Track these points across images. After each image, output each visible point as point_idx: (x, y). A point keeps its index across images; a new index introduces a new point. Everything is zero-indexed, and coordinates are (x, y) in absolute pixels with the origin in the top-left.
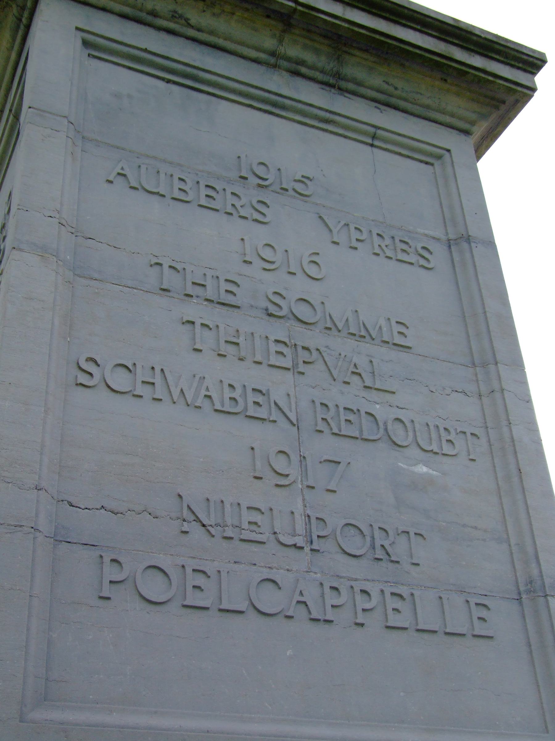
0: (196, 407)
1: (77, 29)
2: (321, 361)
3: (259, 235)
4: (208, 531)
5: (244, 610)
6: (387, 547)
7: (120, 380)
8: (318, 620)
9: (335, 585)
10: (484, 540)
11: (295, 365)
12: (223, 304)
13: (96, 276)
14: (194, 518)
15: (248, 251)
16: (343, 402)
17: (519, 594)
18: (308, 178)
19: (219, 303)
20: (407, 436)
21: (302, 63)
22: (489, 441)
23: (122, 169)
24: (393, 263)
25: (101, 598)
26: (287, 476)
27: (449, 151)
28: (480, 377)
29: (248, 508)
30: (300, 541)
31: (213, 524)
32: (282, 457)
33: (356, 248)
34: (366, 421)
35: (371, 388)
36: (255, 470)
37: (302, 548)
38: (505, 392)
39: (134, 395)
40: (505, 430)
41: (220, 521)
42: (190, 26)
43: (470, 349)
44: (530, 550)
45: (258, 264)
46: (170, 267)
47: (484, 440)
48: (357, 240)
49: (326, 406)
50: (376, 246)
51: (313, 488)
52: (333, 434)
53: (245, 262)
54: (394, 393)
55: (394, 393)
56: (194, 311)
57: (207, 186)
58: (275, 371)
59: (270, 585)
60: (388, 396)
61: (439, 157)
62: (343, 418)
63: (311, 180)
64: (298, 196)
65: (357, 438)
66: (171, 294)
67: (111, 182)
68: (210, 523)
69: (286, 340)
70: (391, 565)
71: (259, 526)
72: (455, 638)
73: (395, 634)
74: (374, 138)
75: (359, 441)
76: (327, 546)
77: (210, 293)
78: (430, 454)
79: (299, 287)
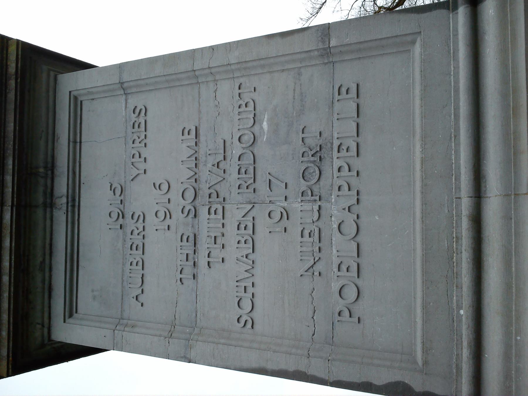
0: (253, 263)
1: (64, 322)
2: (215, 186)
3: (150, 218)
4: (317, 261)
5: (356, 244)
6: (312, 152)
7: (247, 305)
8: (358, 199)
9: (337, 188)
10: (301, 84)
11: (220, 203)
12: (195, 244)
13: (194, 315)
14: (311, 268)
15: (163, 227)
16: (235, 175)
17: (330, 62)
18: (111, 186)
19: (195, 246)
20: (247, 134)
21: (45, 193)
22: (242, 76)
23: (133, 298)
24: (149, 134)
25: (359, 322)
26: (281, 212)
27: (70, 92)
28: (204, 80)
29: (302, 237)
30: (316, 208)
31: (313, 258)
32: (272, 215)
33: (145, 158)
34: (244, 162)
35: (224, 156)
36: (281, 232)
37: (320, 206)
38: (210, 66)
39: (253, 297)
40: (233, 67)
41: (311, 254)
42: (44, 260)
43: (188, 84)
44: (303, 56)
45: (168, 221)
46: (181, 273)
47: (242, 80)
48: (140, 157)
49: (239, 185)
50: (140, 145)
51: (286, 197)
52: (254, 182)
53: (168, 229)
54: (224, 141)
55: (224, 141)
56: (202, 261)
57: (133, 128)
58: (225, 216)
59: (342, 226)
60: (227, 144)
61: (76, 98)
62: (244, 176)
63: (112, 184)
64: (123, 193)
65: (254, 168)
66: (196, 274)
67: (142, 305)
68: (312, 260)
69: (207, 207)
70: (323, 150)
71: (311, 231)
72: (360, 110)
73: (361, 151)
74: (76, 143)
75: (256, 165)
76: (316, 190)
77: (191, 252)
78: (256, 119)
79: (175, 195)
